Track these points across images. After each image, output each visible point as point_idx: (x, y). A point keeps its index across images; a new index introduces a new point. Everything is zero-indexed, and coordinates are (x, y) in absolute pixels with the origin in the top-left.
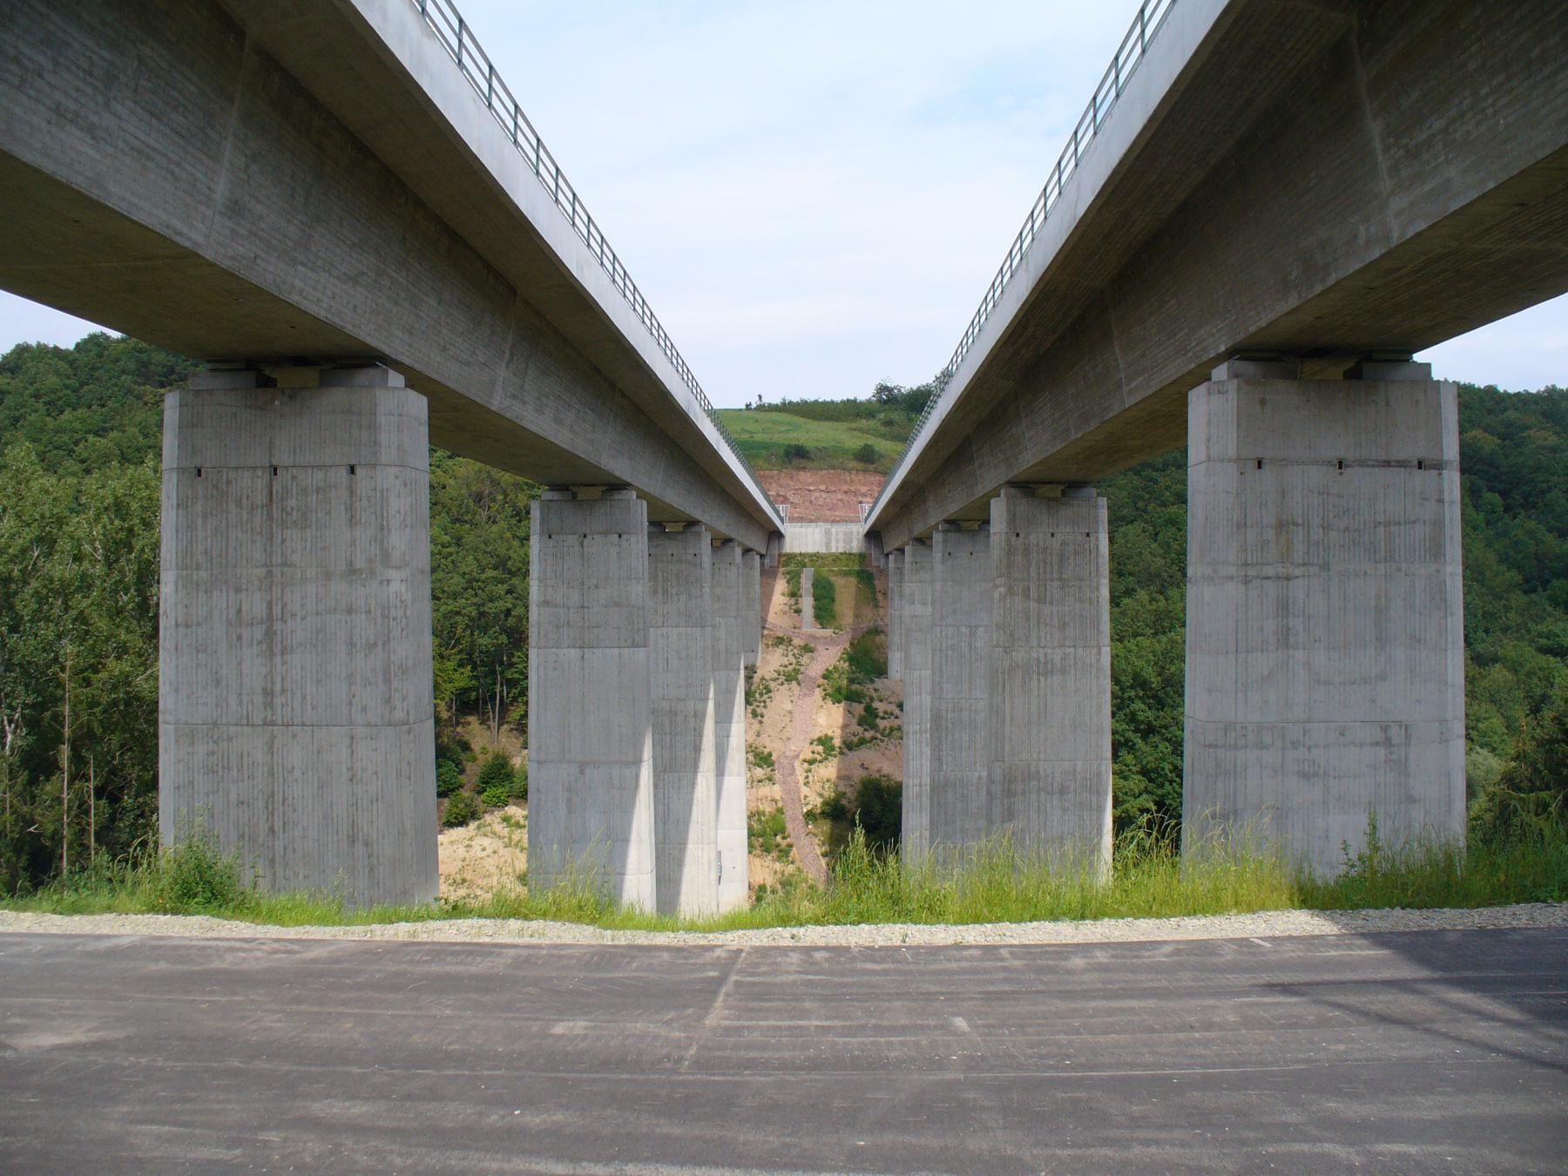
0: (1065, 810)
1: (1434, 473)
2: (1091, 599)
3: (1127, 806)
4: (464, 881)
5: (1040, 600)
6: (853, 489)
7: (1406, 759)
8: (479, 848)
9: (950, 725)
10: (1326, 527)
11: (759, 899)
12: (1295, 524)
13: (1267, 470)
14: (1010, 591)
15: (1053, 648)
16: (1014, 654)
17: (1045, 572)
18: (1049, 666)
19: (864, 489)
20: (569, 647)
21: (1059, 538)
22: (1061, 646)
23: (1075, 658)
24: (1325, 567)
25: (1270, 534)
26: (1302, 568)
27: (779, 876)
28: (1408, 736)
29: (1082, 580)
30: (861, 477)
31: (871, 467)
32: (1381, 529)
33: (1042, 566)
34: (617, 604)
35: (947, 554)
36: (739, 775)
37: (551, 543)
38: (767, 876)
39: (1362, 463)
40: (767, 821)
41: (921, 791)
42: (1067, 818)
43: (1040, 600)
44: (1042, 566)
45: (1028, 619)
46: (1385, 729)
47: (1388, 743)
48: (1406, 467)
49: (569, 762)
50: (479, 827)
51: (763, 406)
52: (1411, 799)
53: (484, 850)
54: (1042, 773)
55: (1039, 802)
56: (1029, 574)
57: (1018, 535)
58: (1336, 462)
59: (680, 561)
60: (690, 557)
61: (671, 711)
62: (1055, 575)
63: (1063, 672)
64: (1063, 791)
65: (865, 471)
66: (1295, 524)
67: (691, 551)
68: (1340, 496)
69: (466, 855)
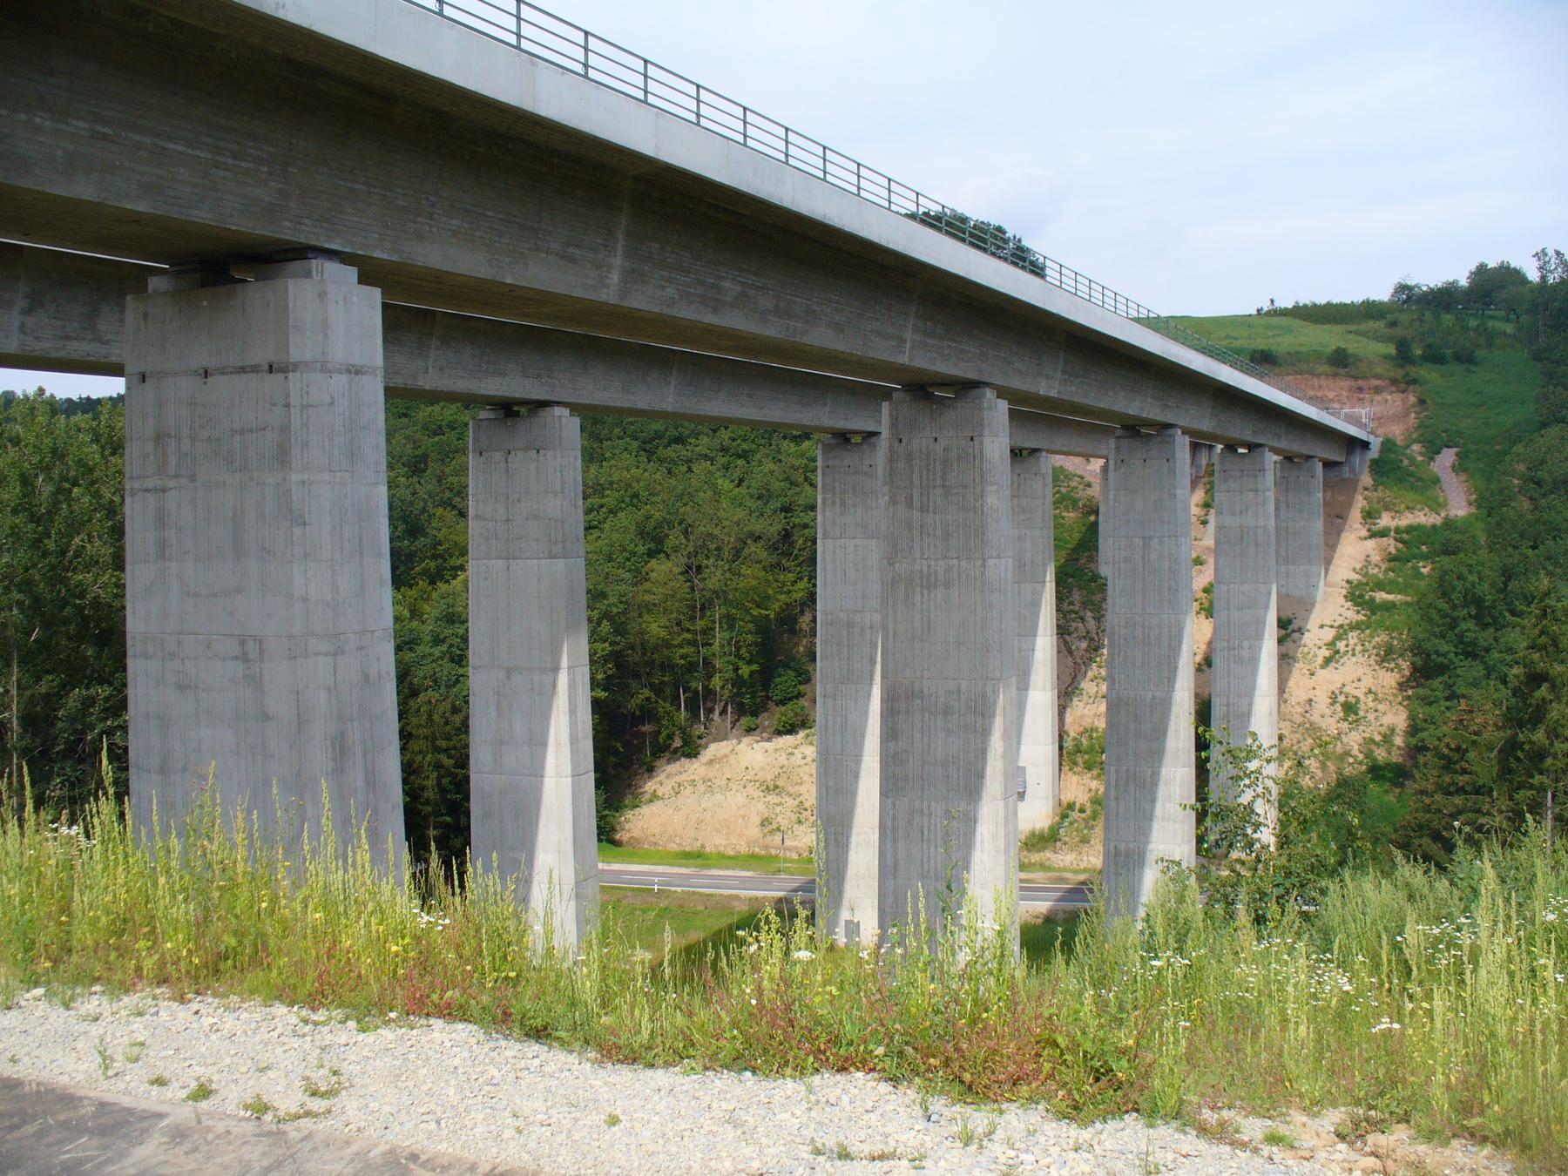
0: (949, 732)
1: (281, 376)
2: (975, 508)
3: (1425, 734)
4: (776, 787)
5: (924, 509)
6: (1319, 395)
7: (261, 675)
8: (800, 756)
9: (1122, 641)
10: (193, 438)
11: (1064, 816)
12: (169, 436)
13: (149, 385)
14: (893, 501)
15: (937, 560)
16: (897, 565)
17: (928, 479)
18: (933, 578)
19: (1331, 395)
20: (497, 558)
21: (942, 443)
22: (945, 558)
23: (959, 570)
24: (193, 478)
25: (150, 447)
26: (174, 480)
27: (1093, 794)
28: (261, 651)
29: (966, 487)
30: (1330, 382)
31: (1342, 371)
32: (237, 438)
33: (925, 472)
34: (536, 517)
35: (1119, 462)
36: (1045, 689)
37: (482, 459)
38: (1080, 794)
39: (222, 371)
40: (1097, 739)
41: (1228, 711)
42: (951, 740)
43: (924, 509)
44: (925, 472)
45: (910, 528)
46: (243, 643)
47: (244, 658)
48: (258, 372)
49: (498, 667)
50: (807, 736)
51: (1275, 311)
52: (266, 717)
53: (804, 758)
54: (926, 693)
55: (923, 723)
56: (911, 483)
57: (900, 441)
58: (202, 371)
59: (857, 473)
60: (866, 469)
61: (848, 623)
62: (939, 482)
63: (947, 585)
64: (946, 712)
65: (1336, 375)
66: (169, 436)
67: (867, 462)
68: (204, 406)
69: (786, 762)
